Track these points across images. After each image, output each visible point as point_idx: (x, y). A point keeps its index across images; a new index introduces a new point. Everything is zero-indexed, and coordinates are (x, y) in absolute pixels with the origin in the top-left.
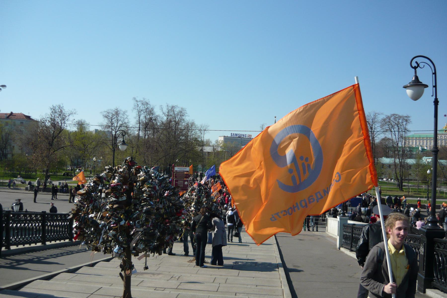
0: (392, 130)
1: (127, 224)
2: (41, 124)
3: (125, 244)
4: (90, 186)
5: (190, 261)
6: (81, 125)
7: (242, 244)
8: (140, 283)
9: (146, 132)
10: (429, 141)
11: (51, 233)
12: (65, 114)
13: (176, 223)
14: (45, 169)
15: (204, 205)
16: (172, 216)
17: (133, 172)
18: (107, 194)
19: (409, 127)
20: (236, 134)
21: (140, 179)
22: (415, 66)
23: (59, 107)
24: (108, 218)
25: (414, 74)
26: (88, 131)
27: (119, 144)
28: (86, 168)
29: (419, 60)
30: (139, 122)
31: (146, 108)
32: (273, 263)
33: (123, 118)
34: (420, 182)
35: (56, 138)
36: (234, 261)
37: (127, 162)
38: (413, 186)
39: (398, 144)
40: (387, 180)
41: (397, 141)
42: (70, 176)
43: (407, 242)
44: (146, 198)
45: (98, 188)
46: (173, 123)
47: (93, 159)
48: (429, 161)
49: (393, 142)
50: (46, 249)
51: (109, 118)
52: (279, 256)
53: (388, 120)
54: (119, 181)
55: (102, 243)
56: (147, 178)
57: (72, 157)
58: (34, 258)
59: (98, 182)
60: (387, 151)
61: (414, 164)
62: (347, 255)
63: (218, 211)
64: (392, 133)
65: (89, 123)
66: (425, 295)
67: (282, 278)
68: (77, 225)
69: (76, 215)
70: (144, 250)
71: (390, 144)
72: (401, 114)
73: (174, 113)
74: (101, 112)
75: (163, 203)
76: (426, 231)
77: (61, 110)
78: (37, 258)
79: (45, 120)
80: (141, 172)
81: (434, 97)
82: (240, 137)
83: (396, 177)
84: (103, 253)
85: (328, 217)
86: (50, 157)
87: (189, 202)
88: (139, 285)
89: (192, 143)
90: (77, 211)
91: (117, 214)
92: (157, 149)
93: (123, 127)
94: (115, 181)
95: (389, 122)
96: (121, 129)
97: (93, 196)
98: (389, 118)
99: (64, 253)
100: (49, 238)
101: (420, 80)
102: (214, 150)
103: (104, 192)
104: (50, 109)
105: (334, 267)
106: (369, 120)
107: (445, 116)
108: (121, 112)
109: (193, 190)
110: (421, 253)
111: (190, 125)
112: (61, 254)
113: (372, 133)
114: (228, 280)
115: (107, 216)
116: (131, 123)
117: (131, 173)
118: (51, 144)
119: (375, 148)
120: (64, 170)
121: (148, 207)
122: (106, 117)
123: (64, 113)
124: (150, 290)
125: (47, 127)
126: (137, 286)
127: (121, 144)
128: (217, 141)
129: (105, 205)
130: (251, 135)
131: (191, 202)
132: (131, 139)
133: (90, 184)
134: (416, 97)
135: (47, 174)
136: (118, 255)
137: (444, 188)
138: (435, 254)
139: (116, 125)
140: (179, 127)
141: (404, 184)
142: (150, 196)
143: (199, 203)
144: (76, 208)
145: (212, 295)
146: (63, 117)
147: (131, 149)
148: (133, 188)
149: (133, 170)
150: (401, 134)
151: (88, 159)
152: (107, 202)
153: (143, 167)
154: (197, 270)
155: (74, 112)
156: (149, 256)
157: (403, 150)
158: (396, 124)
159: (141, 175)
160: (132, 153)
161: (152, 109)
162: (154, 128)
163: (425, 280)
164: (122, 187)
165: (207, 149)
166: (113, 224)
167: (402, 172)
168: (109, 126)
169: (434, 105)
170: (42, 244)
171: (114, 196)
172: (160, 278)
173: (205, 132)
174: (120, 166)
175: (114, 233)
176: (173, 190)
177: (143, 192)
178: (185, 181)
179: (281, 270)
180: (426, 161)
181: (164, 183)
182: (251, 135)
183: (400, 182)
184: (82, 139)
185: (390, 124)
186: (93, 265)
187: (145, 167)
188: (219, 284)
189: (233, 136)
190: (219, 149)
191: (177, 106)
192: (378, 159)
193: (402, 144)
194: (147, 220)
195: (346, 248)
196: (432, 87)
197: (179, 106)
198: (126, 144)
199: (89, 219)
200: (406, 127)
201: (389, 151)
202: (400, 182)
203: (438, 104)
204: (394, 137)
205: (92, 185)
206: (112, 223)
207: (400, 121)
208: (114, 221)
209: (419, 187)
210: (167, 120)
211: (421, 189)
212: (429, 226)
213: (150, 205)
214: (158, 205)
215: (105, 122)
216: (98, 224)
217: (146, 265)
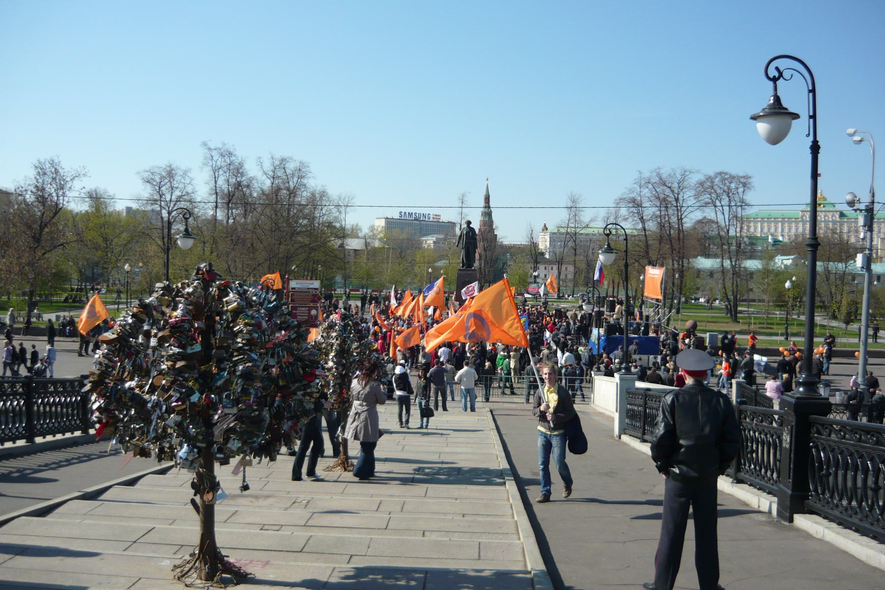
0: (718, 203)
1: (205, 400)
2: (17, 198)
3: (201, 442)
4: (125, 325)
5: (328, 468)
6: (96, 199)
7: (429, 431)
8: (231, 516)
9: (230, 211)
10: (786, 225)
11: (45, 420)
12: (64, 178)
13: (304, 395)
14: (27, 290)
15: (355, 356)
16: (296, 382)
17: (214, 295)
18: (162, 341)
19: (749, 197)
20: (409, 213)
21: (229, 307)
22: (775, 76)
24: (165, 389)
25: (772, 93)
26: (112, 212)
28: (111, 285)
29: (782, 64)
30: (214, 192)
31: (229, 162)
32: (492, 468)
33: (183, 183)
34: (771, 304)
35: (48, 225)
36: (416, 466)
37: (200, 272)
38: (758, 313)
39: (728, 231)
41: (726, 226)
42: (77, 302)
43: (756, 424)
44: (243, 346)
45: (143, 327)
46: (285, 192)
47: (124, 267)
49: (719, 226)
50: (35, 453)
51: (154, 183)
52: (503, 454)
53: (709, 184)
54: (186, 312)
55: (154, 441)
56: (243, 306)
57: (80, 263)
58: (11, 472)
59: (143, 316)
60: (707, 245)
61: (759, 271)
62: (634, 449)
63: (382, 369)
64: (717, 209)
65: (114, 194)
66: (793, 526)
67: (513, 499)
68: (101, 405)
69: (99, 385)
70: (239, 451)
71: (712, 231)
72: (734, 172)
73: (285, 172)
75: (276, 356)
76: (795, 402)
77: (56, 169)
78: (18, 471)
79: (24, 189)
80: (229, 293)
81: (811, 138)
82: (417, 220)
83: (725, 295)
84: (157, 459)
86: (36, 265)
87: (324, 351)
88: (228, 521)
89: (323, 231)
90: (100, 375)
91: (183, 381)
92: (252, 245)
93: (184, 201)
94: (178, 313)
95: (712, 188)
96: (180, 206)
97: (133, 344)
98: (710, 179)
99: (73, 459)
100: (42, 430)
101: (785, 104)
102: (366, 246)
103: (155, 336)
105: (612, 475)
106: (672, 183)
108: (178, 171)
109: (331, 327)
110: (784, 445)
111: (317, 196)
112: (67, 460)
113: (678, 209)
115: (164, 385)
116: (199, 193)
117: (210, 296)
118: (37, 239)
119: (684, 239)
120: (65, 290)
121: (247, 365)
122: (148, 182)
123: (62, 174)
124: (251, 531)
125: (27, 204)
126: (225, 522)
127: (181, 237)
128: (372, 228)
129: (156, 363)
130: (440, 216)
131: (329, 350)
132: (200, 226)
133: (125, 321)
134: (775, 138)
135: (31, 299)
136: (188, 463)
138: (812, 447)
139: (168, 198)
140: (296, 200)
141: (739, 309)
142: (250, 342)
143: (343, 352)
144: (98, 370)
145: (377, 537)
146: (60, 184)
147: (201, 245)
148: (213, 327)
149: (213, 290)
150: (735, 210)
151: (113, 268)
152: (163, 357)
153: (234, 282)
155: (83, 172)
156: (250, 463)
157: (738, 242)
158: (724, 191)
159: (230, 299)
160: (204, 253)
161: (241, 165)
162: (245, 203)
163: (792, 496)
164: (193, 326)
165: (353, 244)
166: (175, 402)
167: (737, 286)
168: (156, 200)
169: (811, 153)
170: (26, 442)
171: (176, 345)
173: (348, 209)
174: (187, 281)
175: (179, 418)
176: (296, 329)
177: (236, 335)
178: (310, 309)
179: (511, 486)
180: (782, 263)
181: (278, 314)
182: (440, 216)
183: (732, 305)
184: (101, 228)
185: (712, 191)
186: (132, 482)
187: (237, 282)
188: (390, 514)
189: (403, 218)
190: (377, 244)
192: (689, 260)
193: (736, 231)
194: (245, 391)
195: (633, 436)
196: (807, 117)
197: (294, 158)
198: (191, 235)
199: (125, 392)
200: (744, 197)
201: (709, 245)
202: (732, 305)
205: (130, 321)
206: (174, 399)
207: (733, 186)
208: (178, 395)
209: (769, 313)
210: (272, 186)
211: (774, 317)
212: (800, 392)
213: (251, 360)
214: (266, 359)
215: (146, 192)
216: (146, 402)
217: (244, 481)
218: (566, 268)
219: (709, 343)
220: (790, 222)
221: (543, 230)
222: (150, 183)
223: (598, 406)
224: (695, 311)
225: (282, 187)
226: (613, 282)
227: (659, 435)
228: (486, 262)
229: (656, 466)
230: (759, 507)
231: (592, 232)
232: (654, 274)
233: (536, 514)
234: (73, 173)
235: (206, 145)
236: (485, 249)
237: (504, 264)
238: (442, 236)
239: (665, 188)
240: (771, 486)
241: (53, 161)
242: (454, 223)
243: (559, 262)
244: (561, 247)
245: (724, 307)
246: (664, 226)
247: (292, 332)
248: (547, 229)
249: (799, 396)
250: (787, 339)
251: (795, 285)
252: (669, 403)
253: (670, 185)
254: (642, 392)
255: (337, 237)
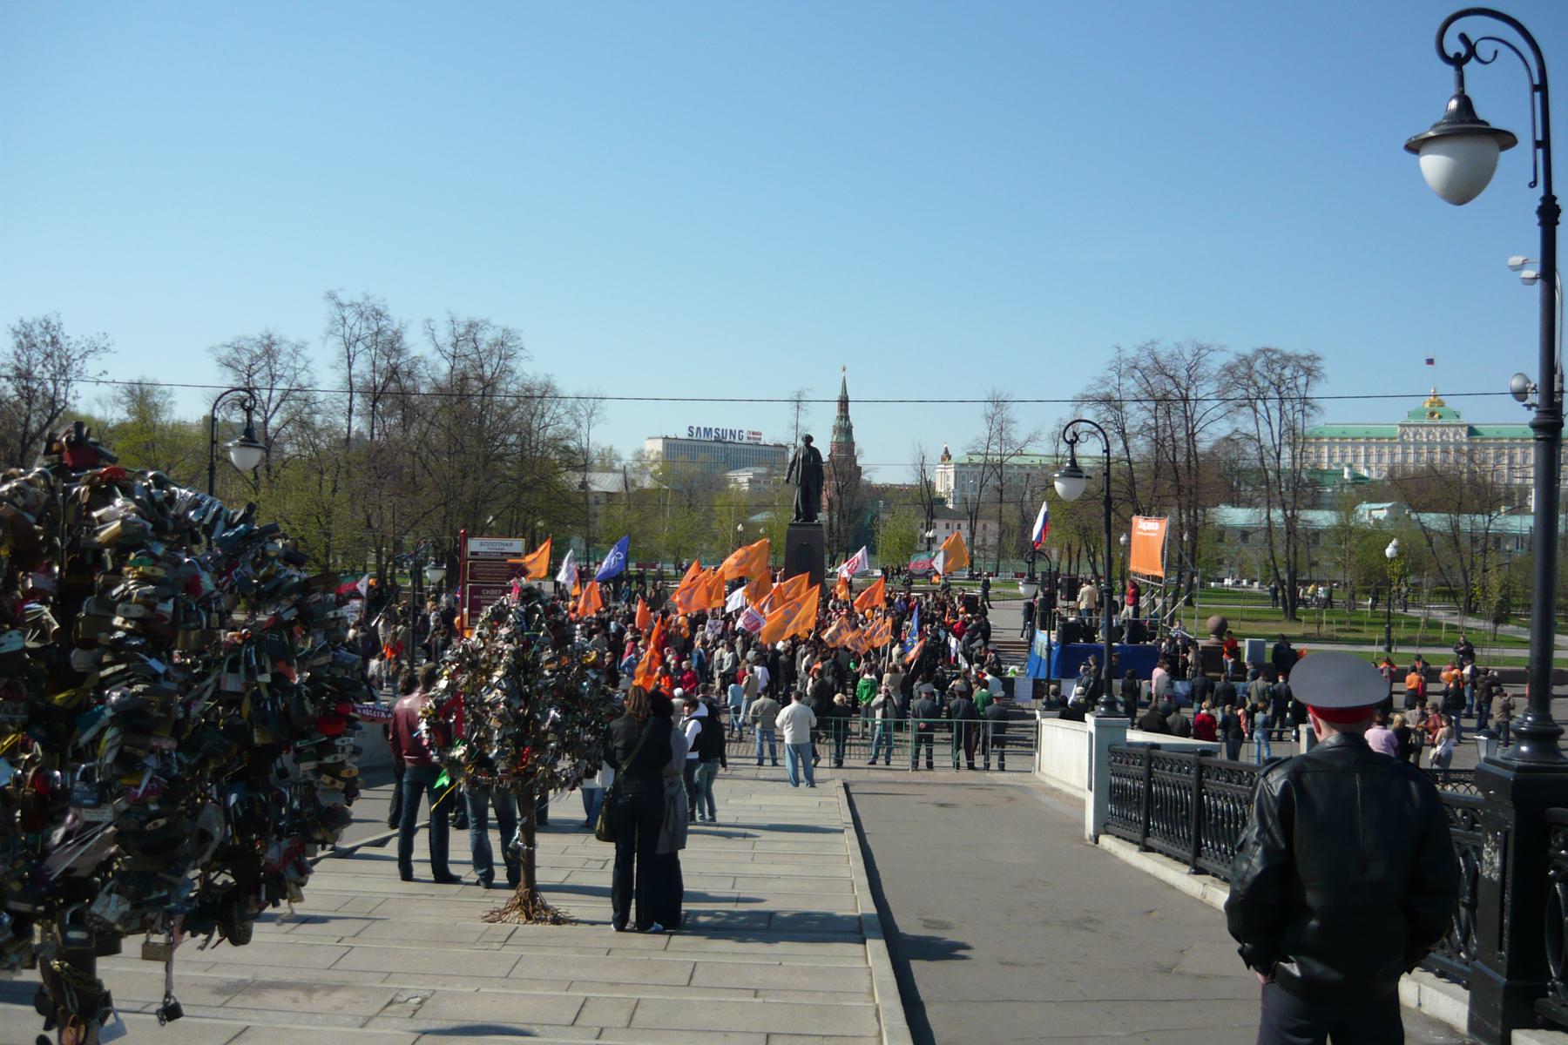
6: (142, 398)
12: (69, 353)
13: (318, 772)
15: (547, 678)
20: (705, 429)
22: (1458, 55)
23: (44, 325)
25: (1453, 88)
27: (230, 445)
29: (1475, 27)
32: (839, 913)
33: (291, 367)
39: (1279, 455)
40: (1238, 582)
44: (125, 638)
48: (1381, 518)
52: (864, 880)
53: (1243, 370)
60: (1235, 484)
62: (1127, 865)
64: (1258, 416)
67: (881, 994)
72: (1288, 350)
73: (477, 348)
74: (211, 348)
75: (242, 668)
76: (1515, 777)
80: (116, 496)
81: (1540, 190)
82: (720, 441)
85: (1042, 717)
98: (1247, 362)
101: (1482, 112)
102: (626, 486)
104: (11, 332)
107: (1430, 362)
108: (284, 346)
109: (499, 617)
113: (1186, 417)
114: (639, 1013)
122: (229, 365)
123: (65, 347)
128: (639, 456)
130: (760, 434)
134: (1462, 191)
137: (1437, 609)
138: (1553, 879)
143: (522, 669)
146: (61, 365)
150: (1291, 418)
154: (513, 962)
155: (104, 344)
161: (398, 336)
163: (1507, 988)
165: (604, 483)
172: (337, 1008)
176: (295, 597)
179: (876, 948)
180: (1370, 515)
182: (760, 434)
187: (151, 474)
189: (694, 438)
190: (647, 483)
191: (488, 324)
194: (128, 763)
195: (1124, 839)
196: (1530, 145)
197: (494, 321)
203: (1559, 219)
204: (1264, 429)
207: (1288, 373)
211: (1363, 612)
212: (1523, 755)
218: (985, 527)
219: (1249, 659)
220: (1380, 445)
221: (943, 459)
222: (231, 366)
223: (1048, 776)
224: (1217, 600)
225: (471, 375)
226: (1069, 549)
227: (1249, 878)
228: (842, 515)
229: (1241, 952)
230: (1420, 1005)
231: (1029, 462)
232: (1149, 531)
233: (933, 1028)
234: (84, 344)
235: (333, 298)
236: (838, 491)
237: (875, 517)
238: (762, 470)
239: (1164, 377)
240: (1447, 961)
241: (48, 323)
242: (786, 447)
243: (972, 513)
244: (975, 490)
245: (1268, 594)
246: (1163, 446)
247: (285, 603)
248: (950, 457)
249: (1521, 763)
250: (1389, 650)
251: (1401, 552)
252: (1276, 794)
253: (1172, 373)
254: (1143, 750)
255: (575, 468)
